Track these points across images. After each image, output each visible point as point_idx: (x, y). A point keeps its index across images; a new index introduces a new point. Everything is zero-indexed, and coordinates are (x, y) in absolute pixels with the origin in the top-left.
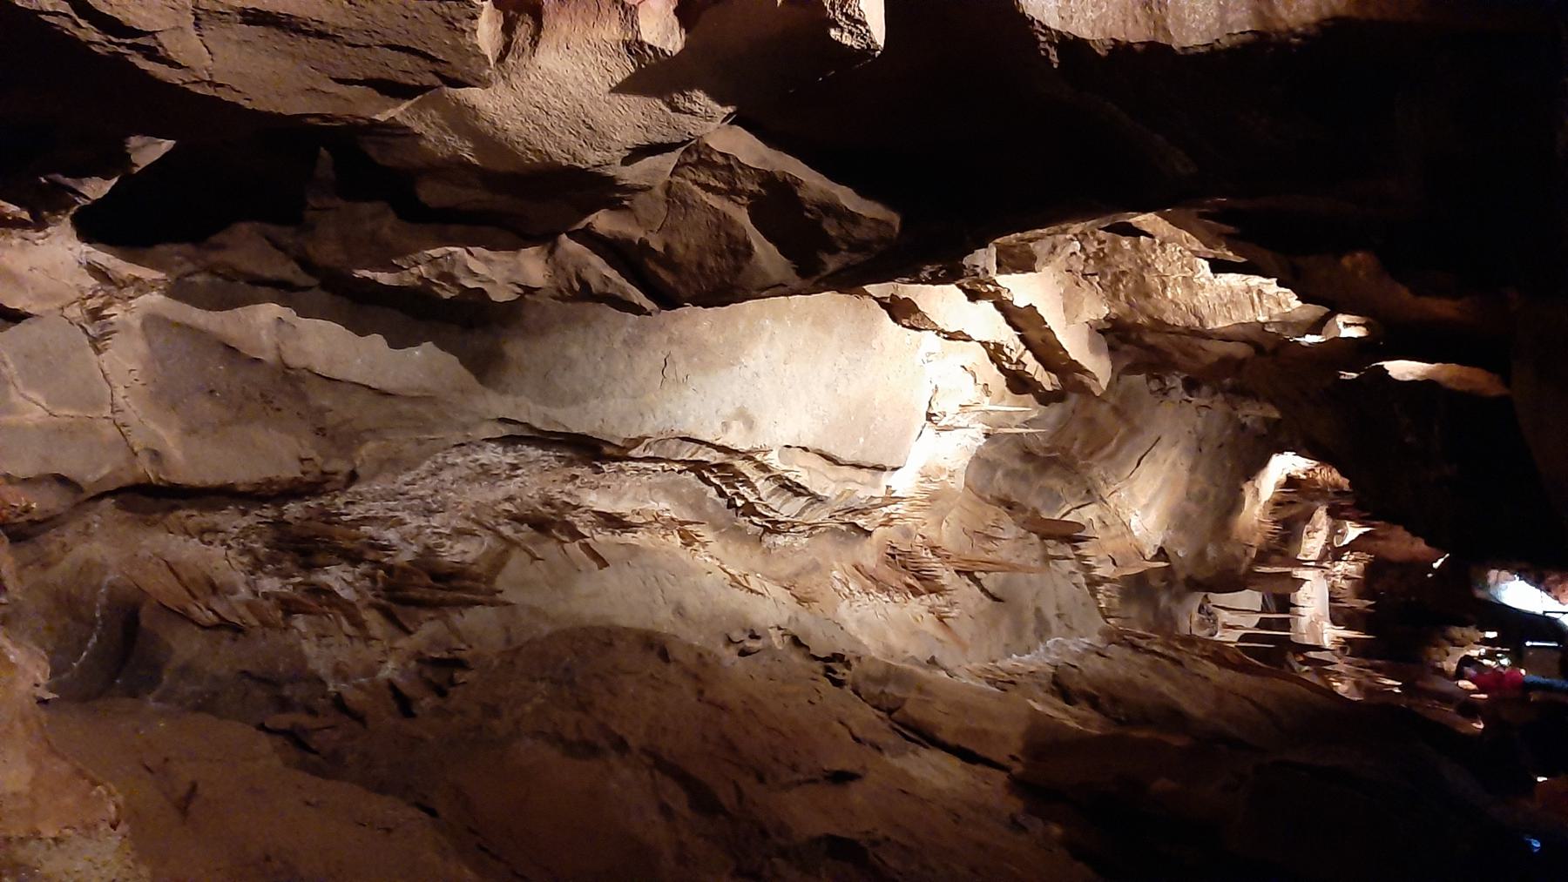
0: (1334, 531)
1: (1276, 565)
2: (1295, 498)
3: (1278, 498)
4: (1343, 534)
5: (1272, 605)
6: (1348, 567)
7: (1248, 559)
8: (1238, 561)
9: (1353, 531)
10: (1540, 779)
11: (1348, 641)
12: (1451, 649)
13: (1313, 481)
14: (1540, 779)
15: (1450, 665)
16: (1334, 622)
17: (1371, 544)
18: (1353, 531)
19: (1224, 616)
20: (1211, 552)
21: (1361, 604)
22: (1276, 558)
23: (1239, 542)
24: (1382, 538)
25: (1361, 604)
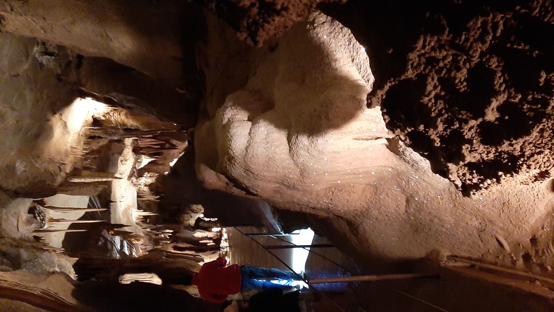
0: (137, 161)
1: (84, 177)
2: (98, 133)
3: (88, 133)
4: (140, 162)
5: (98, 203)
6: (147, 179)
7: (63, 174)
8: (53, 176)
9: (145, 160)
10: (427, 15)
11: (146, 217)
12: (193, 214)
13: (109, 121)
14: (427, 15)
15: (192, 222)
16: (139, 208)
17: (155, 168)
18: (145, 160)
19: (51, 214)
20: (20, 167)
21: (152, 198)
22: (85, 172)
23: (51, 161)
24: (161, 164)
25: (152, 198)
